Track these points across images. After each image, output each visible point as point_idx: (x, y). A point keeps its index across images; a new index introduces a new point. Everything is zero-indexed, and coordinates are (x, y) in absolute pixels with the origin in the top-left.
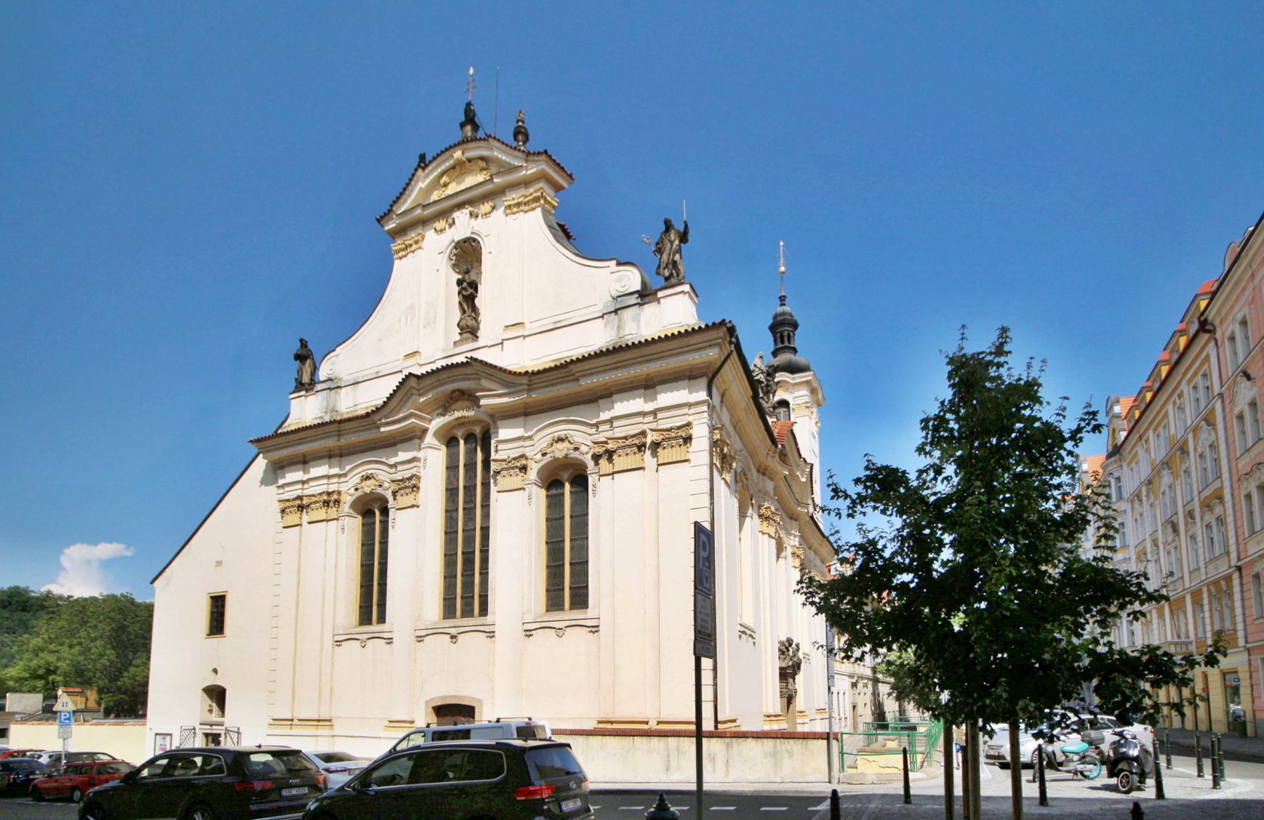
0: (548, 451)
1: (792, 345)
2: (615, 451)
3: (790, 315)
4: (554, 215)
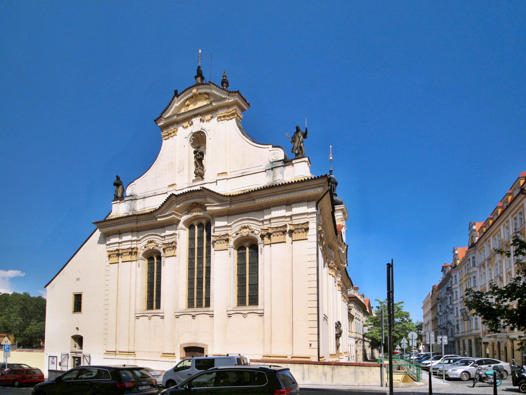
0: (239, 233)
1: (335, 193)
2: (272, 234)
3: (334, 179)
4: (241, 122)
